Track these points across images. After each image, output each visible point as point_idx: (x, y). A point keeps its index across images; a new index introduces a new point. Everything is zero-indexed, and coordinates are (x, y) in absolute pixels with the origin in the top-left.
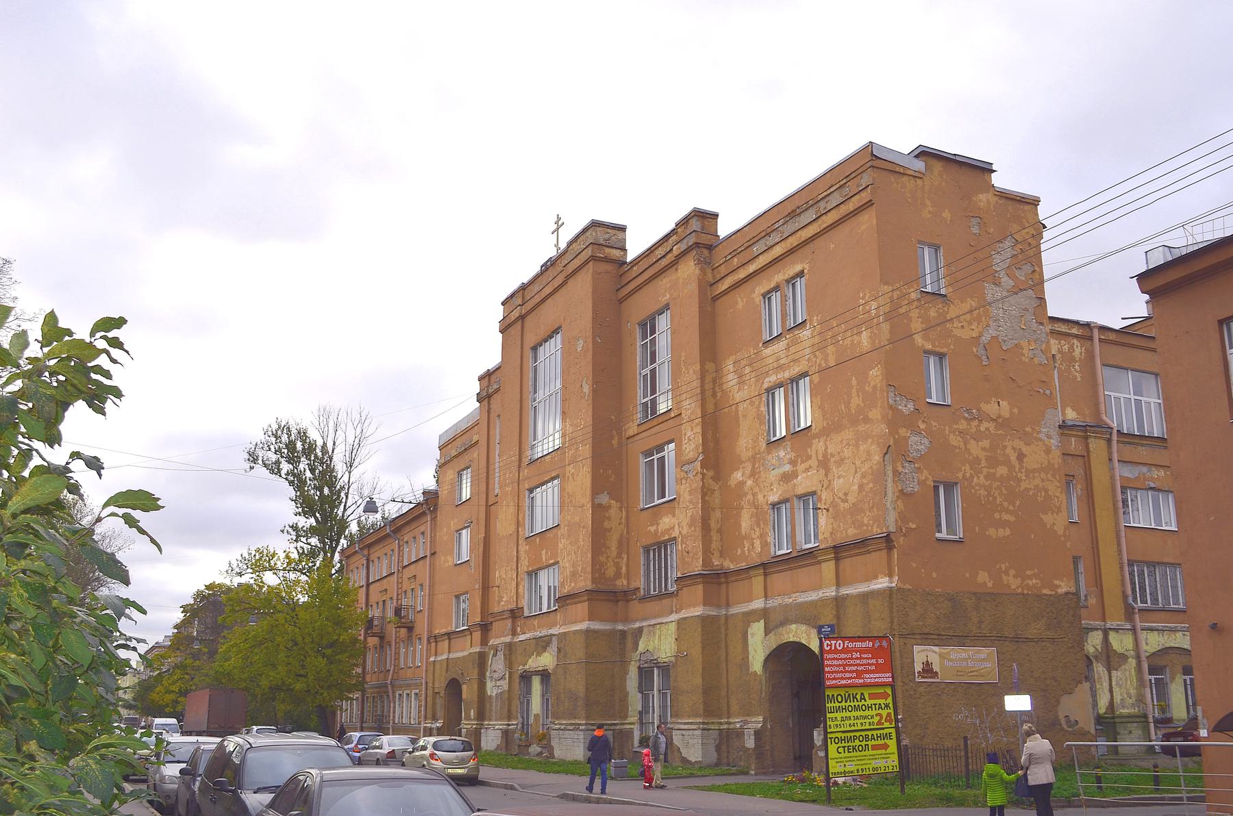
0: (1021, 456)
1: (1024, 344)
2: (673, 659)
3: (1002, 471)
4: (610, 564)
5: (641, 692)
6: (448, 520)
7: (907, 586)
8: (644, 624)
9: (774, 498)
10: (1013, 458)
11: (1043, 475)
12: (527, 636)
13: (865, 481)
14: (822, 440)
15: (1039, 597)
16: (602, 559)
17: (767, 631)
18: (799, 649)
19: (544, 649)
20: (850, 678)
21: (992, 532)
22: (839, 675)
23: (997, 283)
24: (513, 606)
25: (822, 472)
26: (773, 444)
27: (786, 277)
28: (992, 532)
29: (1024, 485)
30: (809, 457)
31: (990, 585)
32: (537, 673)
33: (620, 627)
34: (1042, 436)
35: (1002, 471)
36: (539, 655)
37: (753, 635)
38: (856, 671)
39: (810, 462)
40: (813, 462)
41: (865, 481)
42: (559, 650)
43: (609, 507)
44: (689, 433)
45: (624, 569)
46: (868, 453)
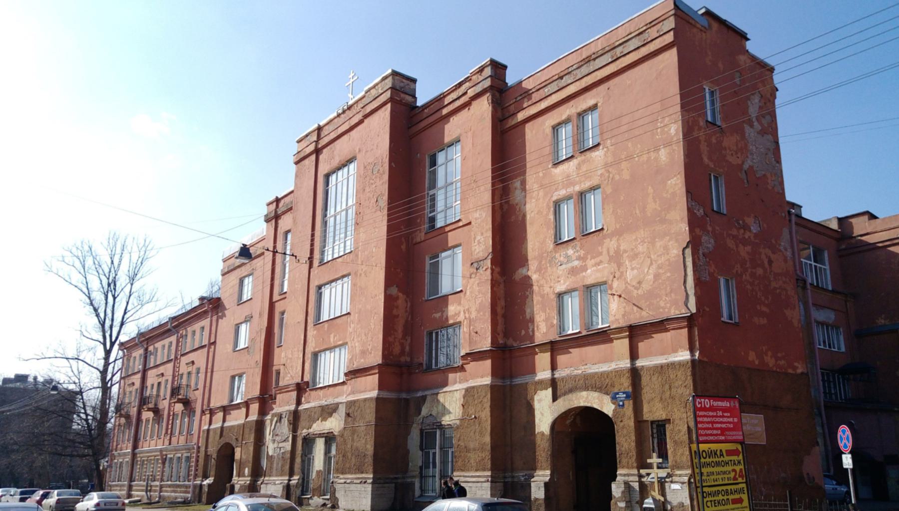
0: (770, 262)
1: (768, 175)
2: (458, 422)
3: (760, 271)
4: (397, 344)
5: (422, 449)
6: (233, 314)
7: (705, 359)
8: (427, 393)
9: (560, 288)
10: (766, 262)
11: (784, 279)
12: (312, 405)
13: (661, 271)
14: (615, 239)
15: (787, 374)
16: (391, 339)
17: (555, 398)
18: (589, 414)
19: (330, 415)
20: (716, 435)
21: (756, 320)
22: (709, 432)
23: (752, 126)
24: (299, 380)
25: (614, 265)
26: (559, 243)
27: (579, 110)
28: (756, 320)
29: (774, 284)
30: (601, 254)
31: (757, 362)
32: (320, 435)
33: (404, 396)
34: (782, 248)
35: (760, 271)
36: (325, 419)
37: (540, 401)
38: (721, 429)
39: (600, 258)
40: (605, 257)
41: (661, 271)
42: (348, 415)
43: (397, 298)
44: (478, 238)
45: (407, 348)
46: (666, 248)
